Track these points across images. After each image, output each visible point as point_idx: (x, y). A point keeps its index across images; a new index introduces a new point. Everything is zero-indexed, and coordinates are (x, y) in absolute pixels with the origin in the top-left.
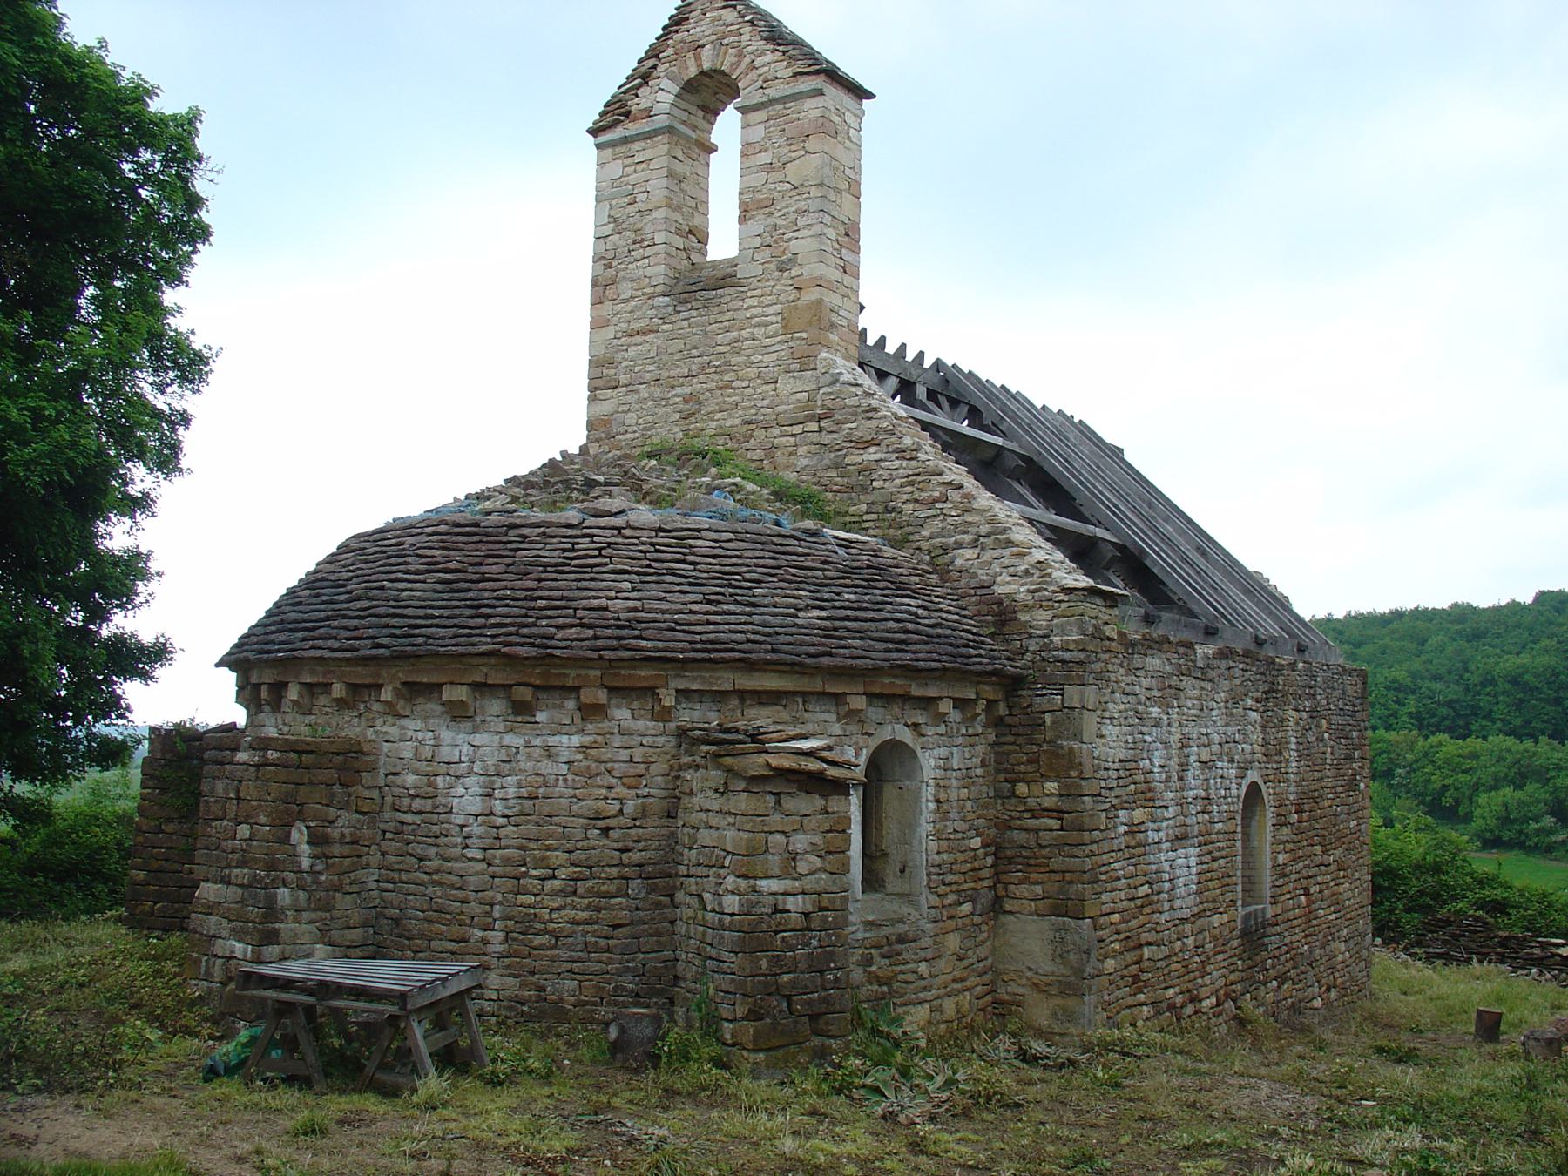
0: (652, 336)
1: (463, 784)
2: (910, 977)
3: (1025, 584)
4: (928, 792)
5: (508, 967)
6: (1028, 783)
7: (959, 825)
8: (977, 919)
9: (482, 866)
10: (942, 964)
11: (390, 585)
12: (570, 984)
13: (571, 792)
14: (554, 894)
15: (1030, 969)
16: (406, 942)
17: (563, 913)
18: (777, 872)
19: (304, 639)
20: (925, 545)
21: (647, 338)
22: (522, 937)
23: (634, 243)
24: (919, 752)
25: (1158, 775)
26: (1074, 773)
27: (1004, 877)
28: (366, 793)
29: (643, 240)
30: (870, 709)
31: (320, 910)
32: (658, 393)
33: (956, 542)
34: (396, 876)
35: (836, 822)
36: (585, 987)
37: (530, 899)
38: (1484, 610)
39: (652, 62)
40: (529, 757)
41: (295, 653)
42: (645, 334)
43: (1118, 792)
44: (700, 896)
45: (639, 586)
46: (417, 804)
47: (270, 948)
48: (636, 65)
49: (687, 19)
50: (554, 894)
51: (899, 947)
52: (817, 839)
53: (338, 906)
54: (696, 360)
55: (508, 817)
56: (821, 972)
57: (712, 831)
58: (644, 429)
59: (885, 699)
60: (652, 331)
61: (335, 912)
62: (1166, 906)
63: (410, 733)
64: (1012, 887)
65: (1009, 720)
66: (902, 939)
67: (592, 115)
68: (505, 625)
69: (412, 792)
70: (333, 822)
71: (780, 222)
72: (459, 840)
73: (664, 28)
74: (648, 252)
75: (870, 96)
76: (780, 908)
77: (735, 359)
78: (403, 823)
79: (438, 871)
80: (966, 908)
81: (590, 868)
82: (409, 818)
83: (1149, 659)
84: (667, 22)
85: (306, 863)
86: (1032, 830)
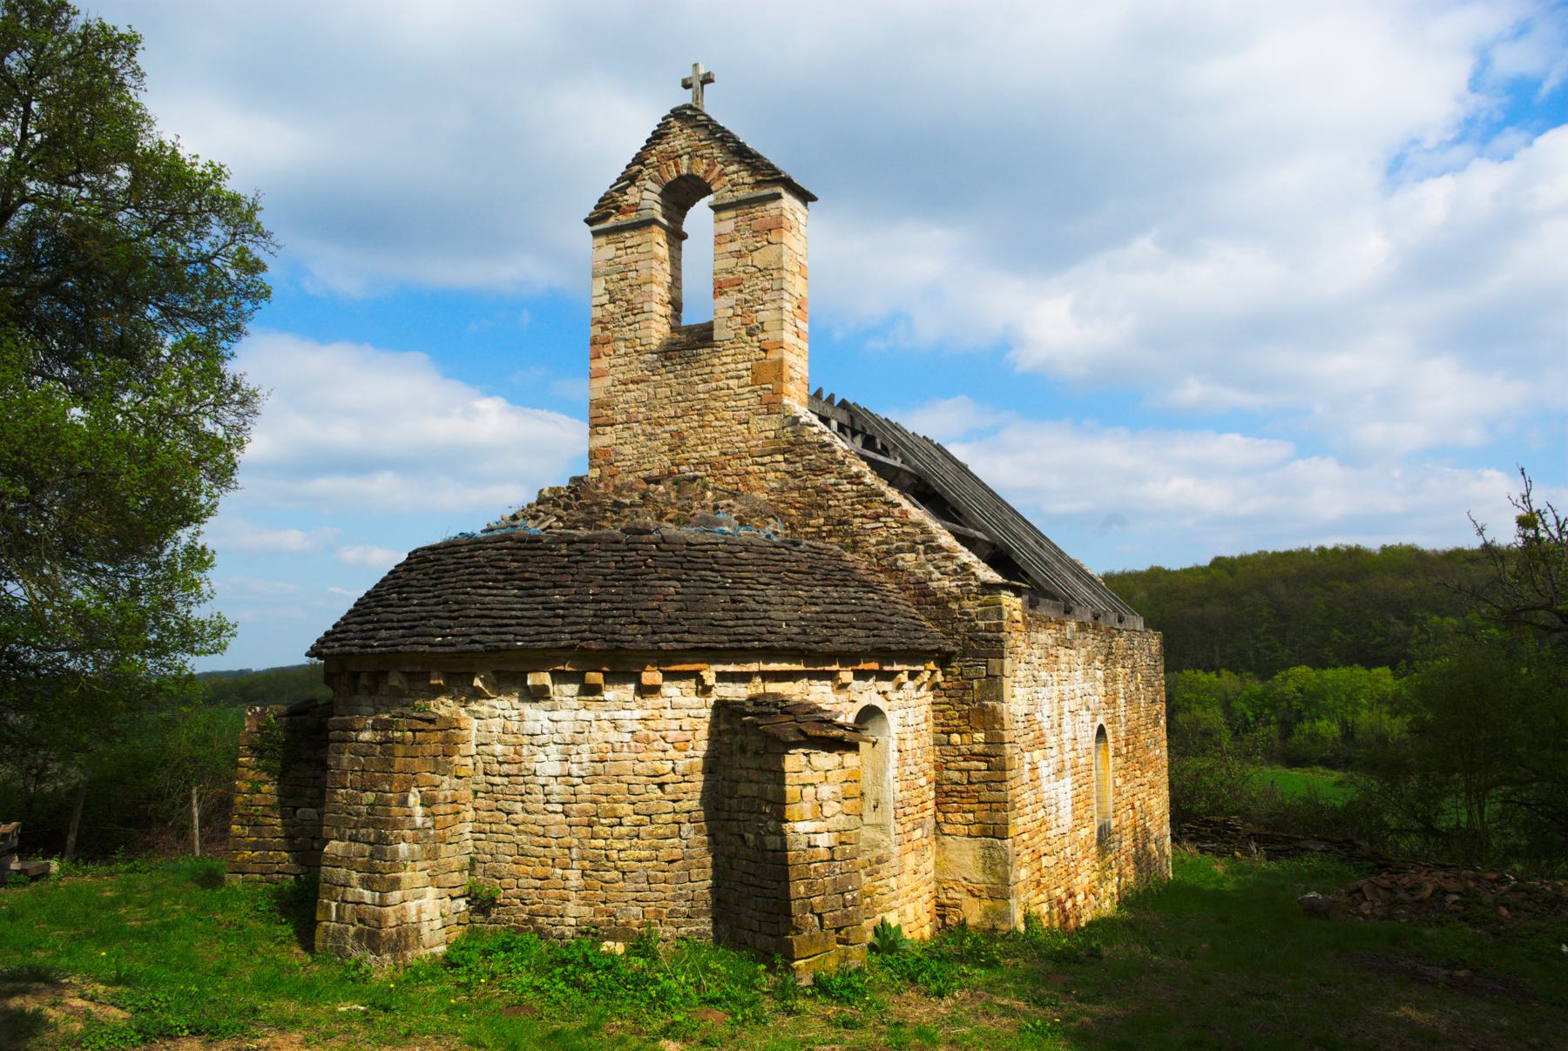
0: (643, 384)
1: (544, 752)
2: (885, 890)
3: (954, 580)
4: (893, 745)
5: (583, 899)
6: (960, 734)
7: (914, 769)
8: (925, 841)
9: (561, 817)
10: (904, 878)
11: (473, 591)
12: (636, 910)
13: (634, 756)
14: (620, 838)
15: (965, 879)
16: (498, 881)
17: (629, 852)
18: (809, 816)
19: (403, 636)
20: (873, 549)
21: (639, 386)
22: (595, 873)
23: (626, 311)
24: (887, 713)
25: (1046, 725)
26: (997, 726)
27: (943, 807)
28: (463, 761)
29: (633, 309)
30: (855, 682)
31: (430, 859)
32: (649, 429)
33: (897, 548)
34: (487, 827)
35: (850, 775)
36: (648, 912)
37: (601, 843)
38: (1175, 572)
39: (637, 168)
40: (600, 728)
41: (399, 648)
42: (637, 383)
43: (1024, 738)
44: (742, 837)
45: (681, 590)
46: (505, 768)
47: (394, 893)
48: (624, 169)
49: (667, 134)
50: (620, 838)
51: (877, 866)
52: (837, 789)
53: (443, 855)
54: (681, 404)
55: (582, 777)
56: (842, 894)
57: (752, 785)
58: (639, 458)
59: (861, 675)
60: (643, 381)
61: (440, 860)
62: (1054, 825)
63: (498, 712)
64: (949, 815)
65: (944, 685)
66: (879, 861)
67: (589, 209)
68: (578, 623)
69: (500, 759)
70: (438, 786)
71: (749, 297)
72: (542, 797)
73: (648, 141)
74: (638, 318)
75: (814, 199)
76: (812, 844)
77: (712, 404)
78: (492, 785)
79: (523, 823)
80: (918, 833)
81: (650, 816)
82: (497, 780)
83: (1039, 635)
84: (650, 136)
85: (419, 821)
86: (965, 770)
